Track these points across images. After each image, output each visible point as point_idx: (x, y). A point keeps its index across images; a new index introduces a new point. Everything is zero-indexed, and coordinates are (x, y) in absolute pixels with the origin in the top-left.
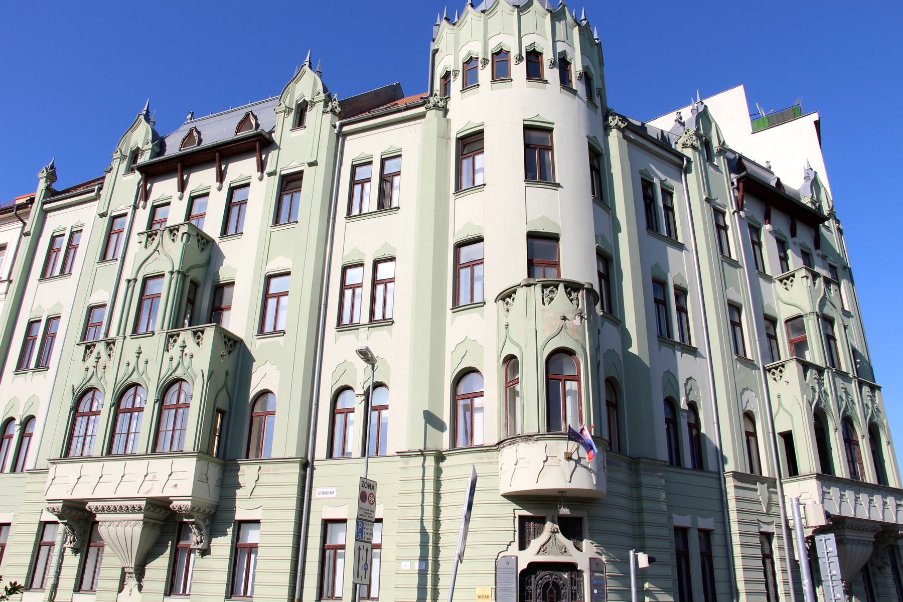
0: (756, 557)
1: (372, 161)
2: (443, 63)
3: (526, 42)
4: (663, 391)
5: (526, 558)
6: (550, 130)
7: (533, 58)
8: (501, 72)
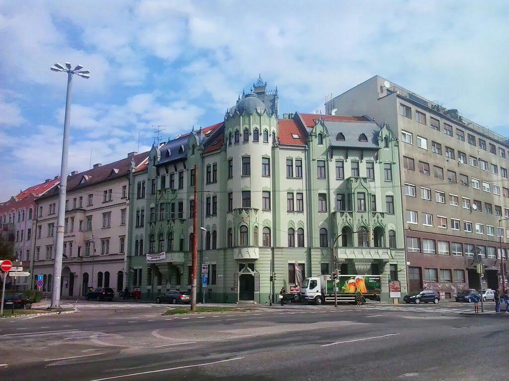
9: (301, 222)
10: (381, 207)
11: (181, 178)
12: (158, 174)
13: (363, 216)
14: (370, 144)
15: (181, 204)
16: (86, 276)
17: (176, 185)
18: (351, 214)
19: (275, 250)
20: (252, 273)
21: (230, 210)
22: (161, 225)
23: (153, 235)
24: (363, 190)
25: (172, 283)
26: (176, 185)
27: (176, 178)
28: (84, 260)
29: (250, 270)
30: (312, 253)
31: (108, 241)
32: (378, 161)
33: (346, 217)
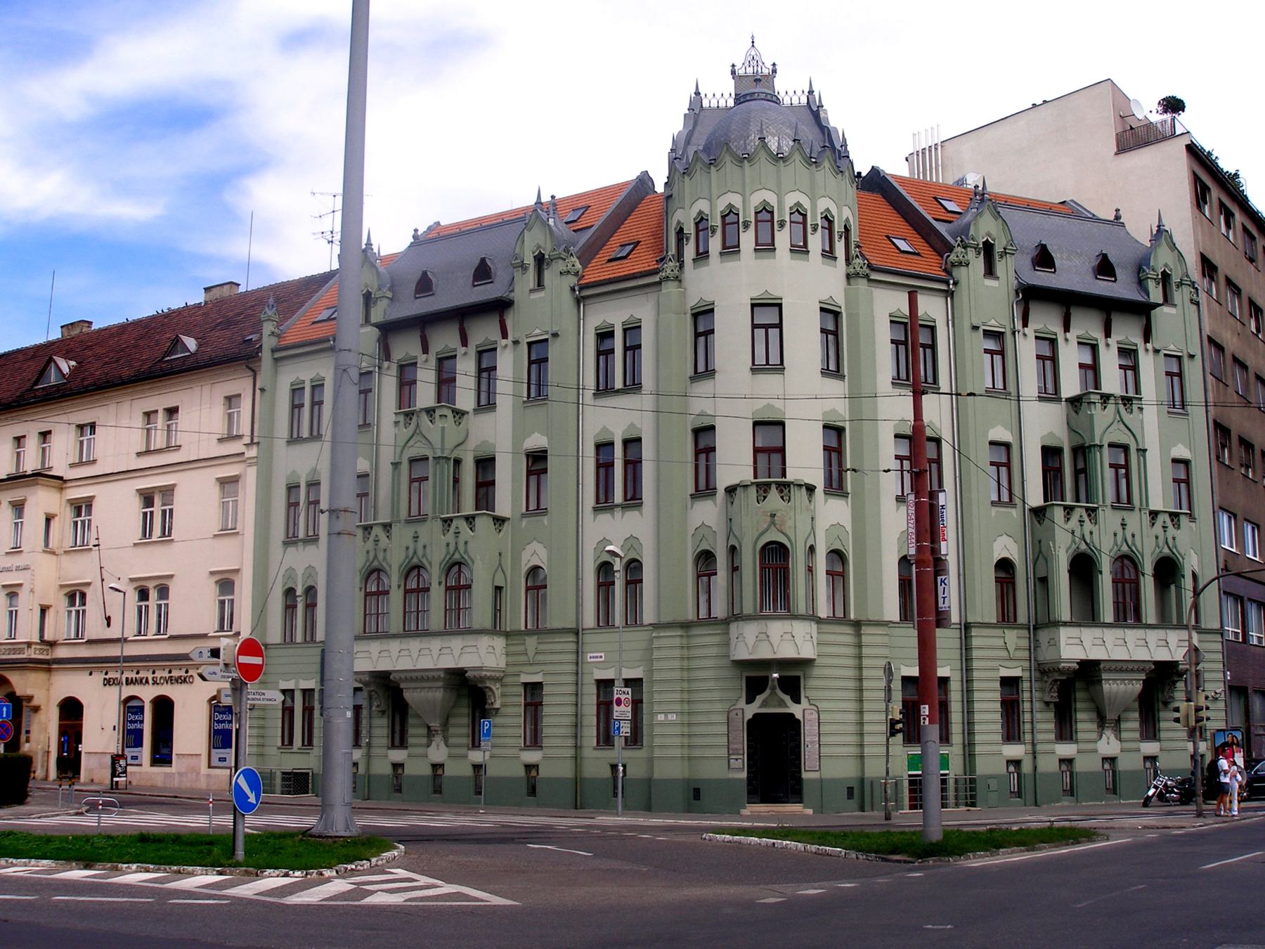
0: (869, 723)
4: (899, 551)
5: (751, 710)
9: (631, 542)
10: (1159, 494)
11: (486, 372)
12: (386, 353)
13: (1127, 521)
14: (1122, 288)
15: (486, 464)
16: (71, 710)
17: (465, 397)
18: (1091, 511)
19: (974, 632)
20: (796, 710)
21: (705, 489)
22: (416, 538)
23: (418, 567)
24: (1124, 438)
25: (451, 741)
26: (465, 397)
27: (466, 368)
28: (62, 653)
29: (787, 698)
30: (975, 642)
31: (164, 592)
32: (1149, 346)
33: (376, 541)
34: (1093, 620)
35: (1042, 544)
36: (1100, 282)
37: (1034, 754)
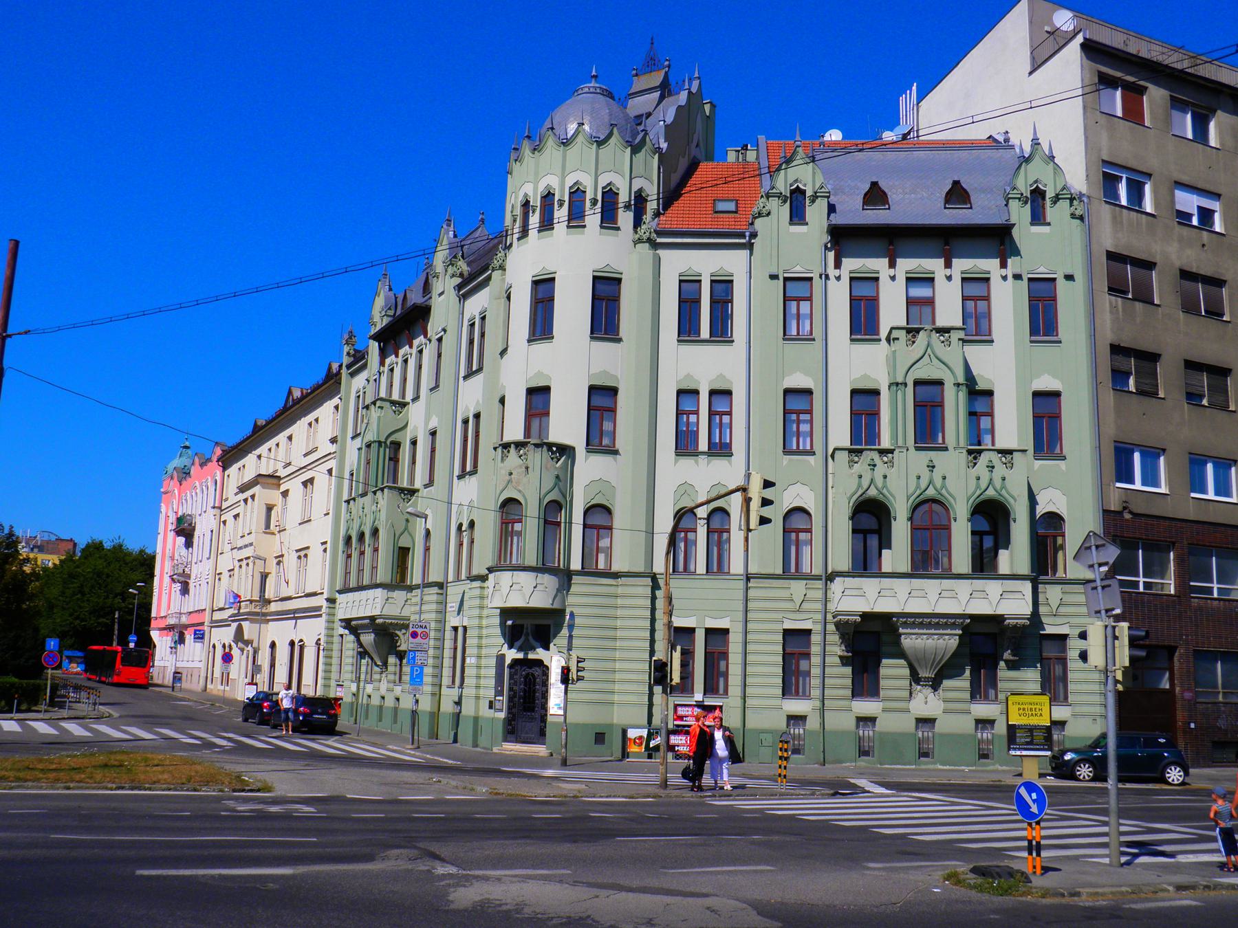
1: (415, 426)
2: (513, 201)
3: (603, 181)
6: (619, 281)
7: (609, 198)
8: (576, 217)
22: (932, 467)
34: (865, 569)
35: (273, 513)
36: (868, 211)
37: (822, 710)
